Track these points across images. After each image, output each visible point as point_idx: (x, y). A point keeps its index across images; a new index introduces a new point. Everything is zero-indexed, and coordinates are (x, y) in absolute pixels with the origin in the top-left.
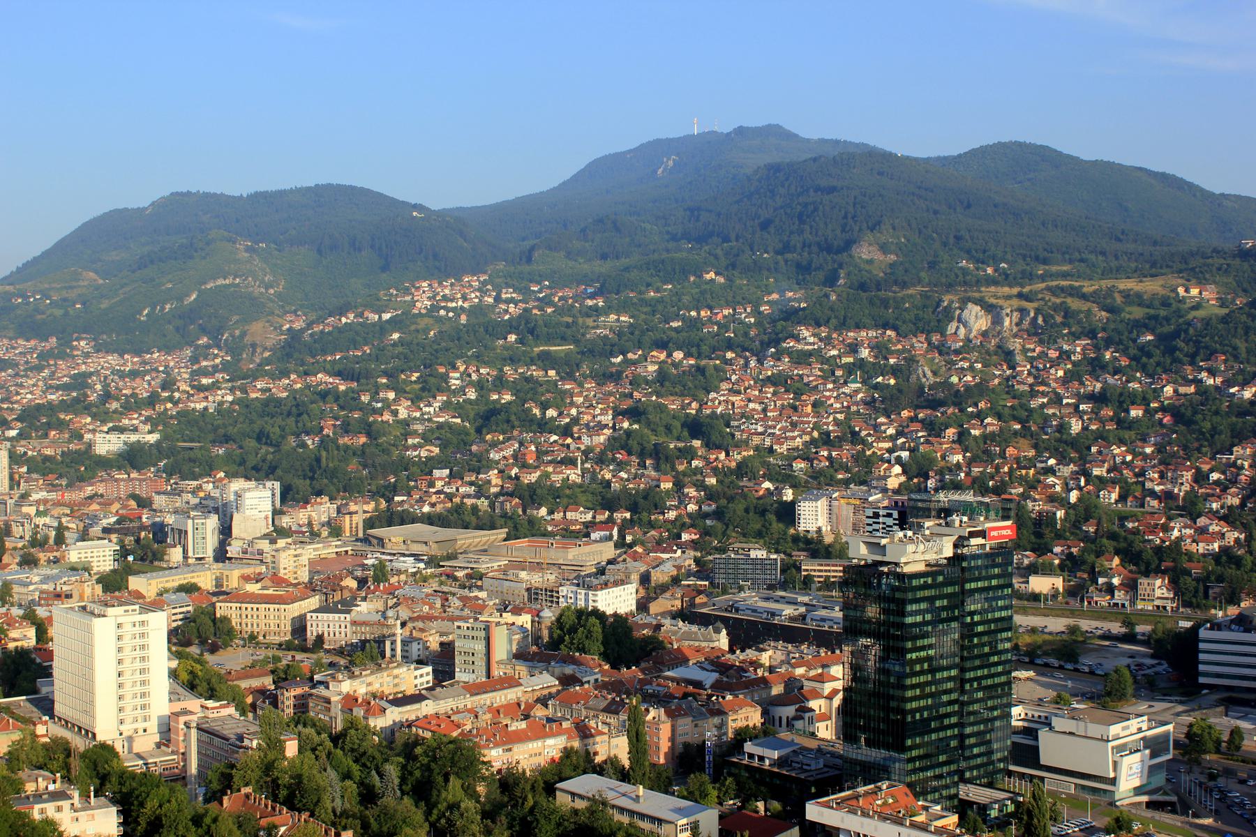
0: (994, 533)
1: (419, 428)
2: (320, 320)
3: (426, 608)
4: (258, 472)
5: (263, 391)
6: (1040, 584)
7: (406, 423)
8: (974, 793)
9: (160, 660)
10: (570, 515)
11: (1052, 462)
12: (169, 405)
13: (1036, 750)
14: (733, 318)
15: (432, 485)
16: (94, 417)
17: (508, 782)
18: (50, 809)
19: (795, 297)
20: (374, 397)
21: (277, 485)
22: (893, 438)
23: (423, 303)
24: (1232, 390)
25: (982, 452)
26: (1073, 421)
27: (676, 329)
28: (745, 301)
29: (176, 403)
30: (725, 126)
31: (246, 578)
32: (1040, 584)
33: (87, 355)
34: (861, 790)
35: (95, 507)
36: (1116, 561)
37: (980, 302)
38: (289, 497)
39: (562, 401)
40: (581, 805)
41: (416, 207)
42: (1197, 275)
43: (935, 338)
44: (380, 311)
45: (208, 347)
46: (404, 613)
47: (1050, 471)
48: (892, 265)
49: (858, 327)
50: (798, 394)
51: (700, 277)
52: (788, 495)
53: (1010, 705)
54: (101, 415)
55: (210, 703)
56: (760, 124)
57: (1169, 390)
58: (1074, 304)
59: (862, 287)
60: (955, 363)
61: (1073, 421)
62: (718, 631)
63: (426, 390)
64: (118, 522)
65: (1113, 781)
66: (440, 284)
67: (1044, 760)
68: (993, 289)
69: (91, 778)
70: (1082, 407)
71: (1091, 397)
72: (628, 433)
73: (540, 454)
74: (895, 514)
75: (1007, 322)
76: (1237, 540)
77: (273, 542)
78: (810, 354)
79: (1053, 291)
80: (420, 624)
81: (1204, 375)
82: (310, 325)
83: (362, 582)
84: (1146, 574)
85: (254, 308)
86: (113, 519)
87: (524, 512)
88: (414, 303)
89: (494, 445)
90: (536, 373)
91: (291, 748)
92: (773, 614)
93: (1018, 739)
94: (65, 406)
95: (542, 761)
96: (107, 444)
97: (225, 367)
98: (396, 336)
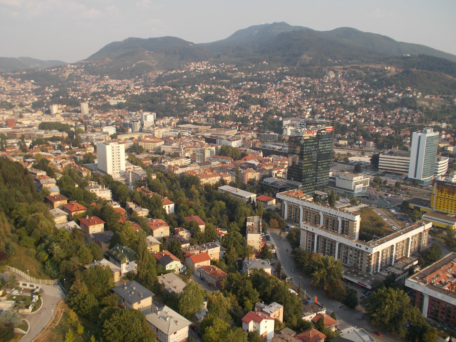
0: (328, 130)
1: (190, 100)
2: (166, 72)
3: (190, 145)
4: (151, 110)
5: (152, 90)
6: (341, 142)
7: (187, 99)
8: (317, 192)
9: (123, 156)
10: (227, 123)
11: (348, 112)
12: (128, 93)
13: (335, 183)
14: (270, 73)
15: (193, 115)
16: (110, 95)
17: (207, 187)
18: (94, 190)
19: (286, 69)
20: (180, 92)
21: (155, 114)
22: (308, 105)
23: (192, 68)
24: (396, 94)
25: (329, 108)
26: (354, 102)
27: (255, 76)
28: (273, 69)
29: (130, 92)
30: (271, 22)
31: (146, 137)
32: (341, 142)
33: (107, 80)
34: (290, 191)
35: (110, 118)
36: (361, 137)
37: (333, 70)
38: (159, 117)
39: (226, 94)
40: (223, 192)
41: (192, 43)
42: (390, 64)
43: (321, 80)
44: (182, 70)
45: (138, 78)
46: (184, 146)
47: (347, 114)
48: (311, 60)
49: (301, 76)
50: (285, 93)
51: (262, 62)
52: (281, 119)
53: (329, 172)
54: (112, 95)
55: (135, 166)
56: (280, 22)
57: (380, 94)
58: (357, 71)
59: (303, 66)
60: (325, 86)
61: (354, 102)
62: (260, 152)
63: (193, 90)
64: (116, 122)
65: (353, 191)
66: (197, 63)
67: (337, 185)
68: (336, 67)
69: (104, 182)
70: (357, 98)
71: (359, 96)
72: (242, 103)
73: (220, 107)
74: (305, 124)
75: (339, 76)
76: (393, 133)
77: (154, 128)
78: (288, 83)
79: (352, 67)
80: (188, 149)
81: (389, 90)
82: (164, 73)
83: (175, 138)
84: (369, 141)
85: (149, 69)
86: (114, 121)
87: (216, 122)
88: (190, 68)
89: (209, 105)
90: (220, 87)
91: (154, 177)
92: (274, 148)
93: (330, 180)
94: (102, 92)
95: (215, 182)
96: (113, 102)
97: (143, 84)
98: (185, 77)
